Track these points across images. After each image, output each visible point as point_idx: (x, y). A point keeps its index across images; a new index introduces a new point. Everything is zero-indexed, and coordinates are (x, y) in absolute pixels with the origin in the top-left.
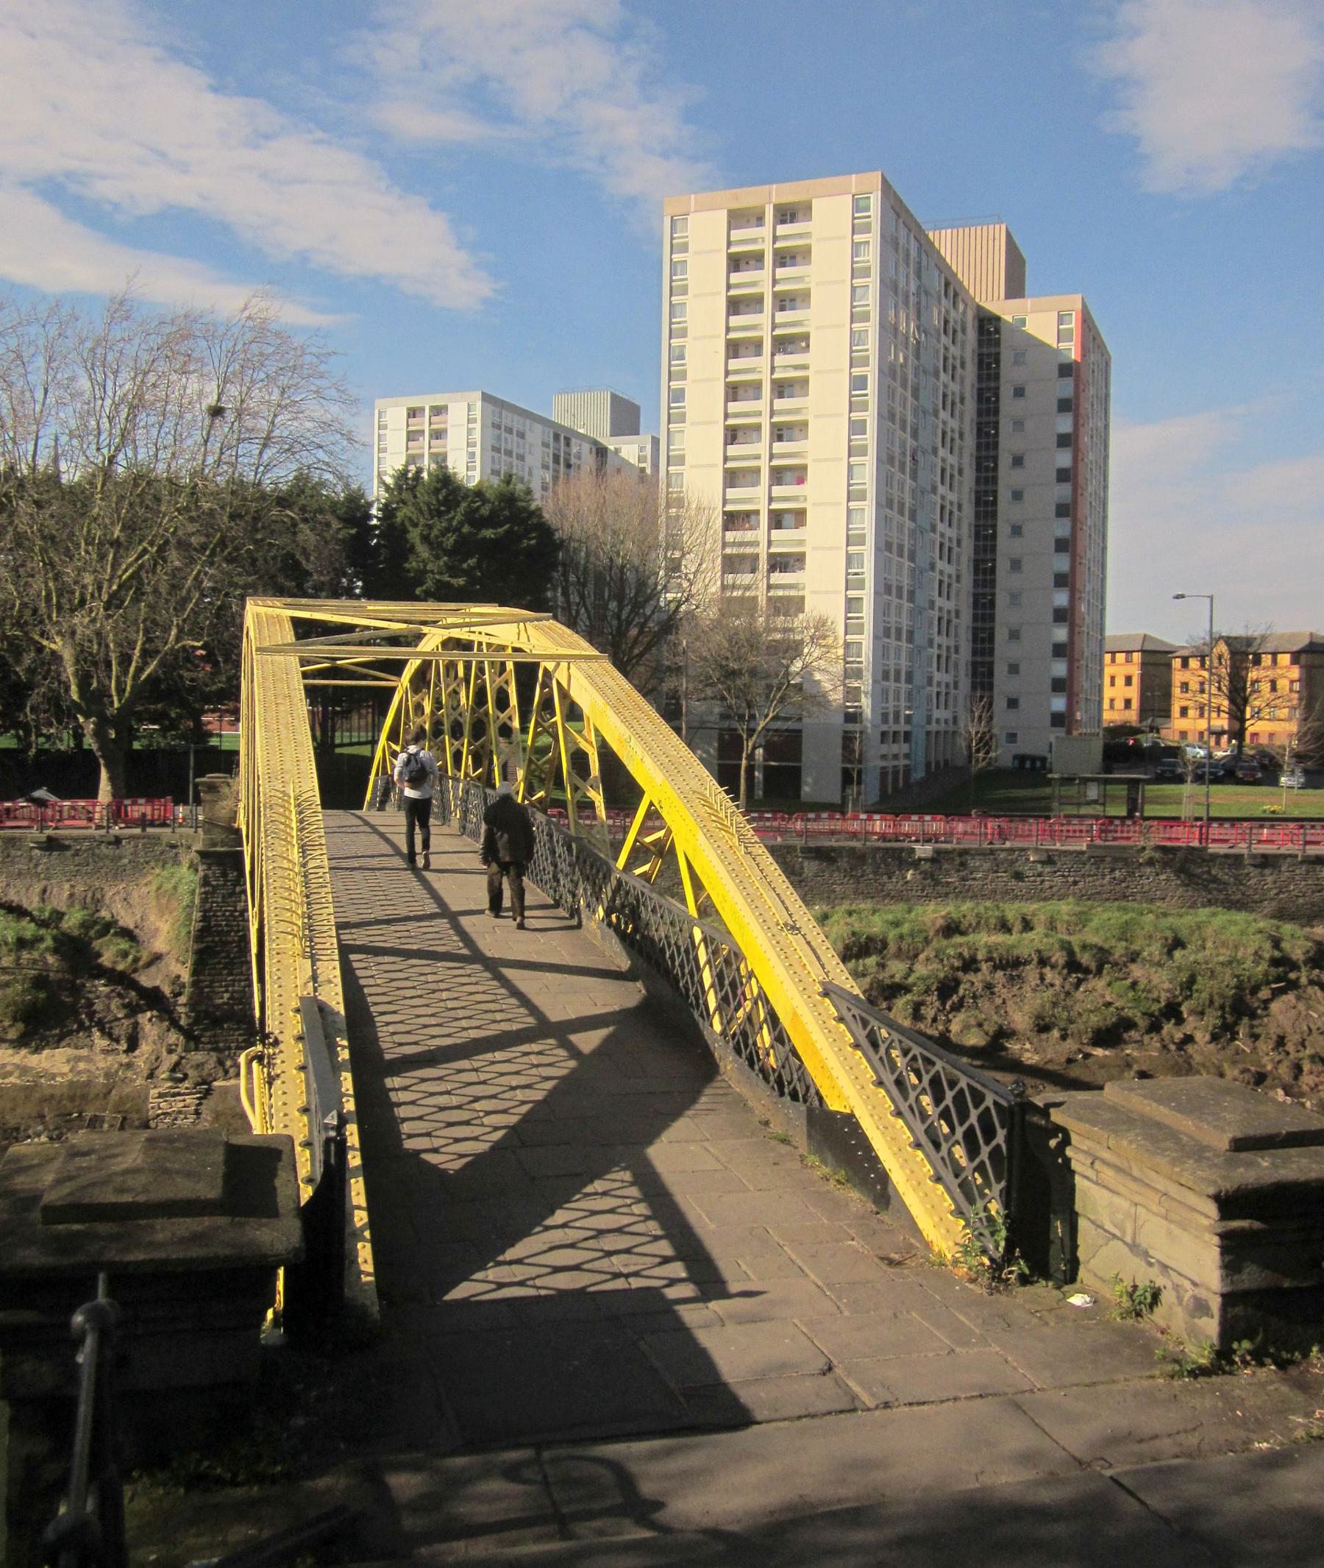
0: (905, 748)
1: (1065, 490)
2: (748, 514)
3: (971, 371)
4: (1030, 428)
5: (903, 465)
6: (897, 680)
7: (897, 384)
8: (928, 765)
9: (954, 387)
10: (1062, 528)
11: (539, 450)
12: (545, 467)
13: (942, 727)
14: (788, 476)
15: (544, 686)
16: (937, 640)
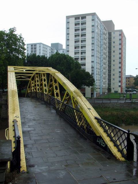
0: (99, 90)
1: (120, 55)
2: (78, 58)
3: (107, 40)
4: (116, 47)
5: (99, 52)
6: (98, 81)
7: (98, 41)
8: (102, 92)
9: (105, 42)
10: (120, 47)
11: (49, 53)
12: (50, 50)
13: (104, 87)
14: (83, 53)
15: (51, 77)
16: (103, 75)
